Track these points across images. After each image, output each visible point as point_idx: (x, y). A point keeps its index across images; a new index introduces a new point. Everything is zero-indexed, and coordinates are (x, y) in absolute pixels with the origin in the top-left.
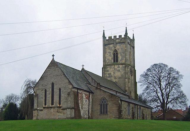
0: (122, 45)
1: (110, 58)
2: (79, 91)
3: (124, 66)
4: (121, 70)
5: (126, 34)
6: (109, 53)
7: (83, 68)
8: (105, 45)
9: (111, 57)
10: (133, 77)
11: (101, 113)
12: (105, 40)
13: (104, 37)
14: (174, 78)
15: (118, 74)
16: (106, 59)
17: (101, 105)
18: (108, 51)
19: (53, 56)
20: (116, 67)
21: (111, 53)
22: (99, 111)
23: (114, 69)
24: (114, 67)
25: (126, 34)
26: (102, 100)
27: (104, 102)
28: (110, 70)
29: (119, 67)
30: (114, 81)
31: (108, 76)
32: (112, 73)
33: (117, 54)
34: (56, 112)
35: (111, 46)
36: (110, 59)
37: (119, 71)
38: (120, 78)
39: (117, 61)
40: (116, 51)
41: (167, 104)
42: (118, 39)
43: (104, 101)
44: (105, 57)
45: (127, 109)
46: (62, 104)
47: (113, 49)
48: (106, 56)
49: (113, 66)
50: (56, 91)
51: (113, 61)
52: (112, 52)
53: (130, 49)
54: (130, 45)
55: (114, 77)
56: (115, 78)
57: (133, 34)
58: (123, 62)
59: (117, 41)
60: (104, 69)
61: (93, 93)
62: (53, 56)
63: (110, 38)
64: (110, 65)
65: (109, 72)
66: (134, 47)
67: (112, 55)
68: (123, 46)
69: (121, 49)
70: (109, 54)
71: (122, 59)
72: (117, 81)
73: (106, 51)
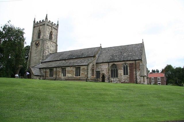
5: (46, 18)
7: (101, 46)
13: (34, 22)
25: (46, 18)
32: (49, 47)
40: (51, 32)
62: (101, 44)
63: (37, 22)
71: (54, 40)
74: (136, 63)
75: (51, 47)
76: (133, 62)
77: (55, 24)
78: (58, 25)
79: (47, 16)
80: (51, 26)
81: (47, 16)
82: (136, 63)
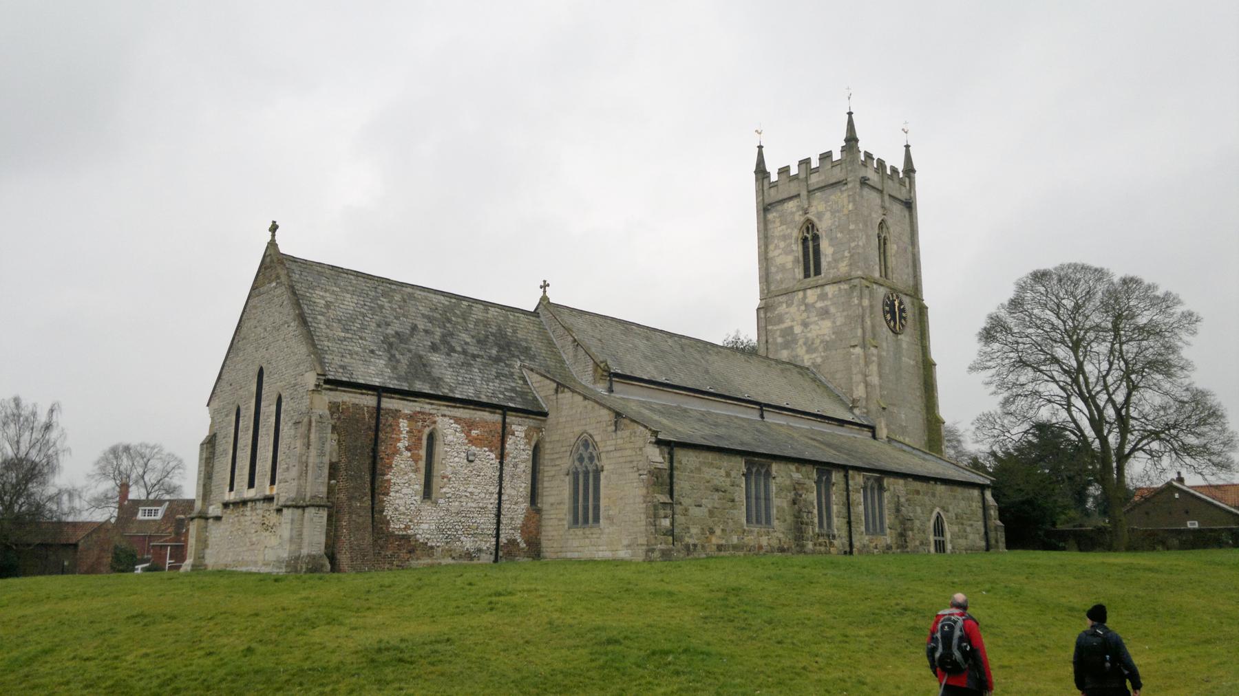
0: (833, 197)
1: (788, 257)
2: (389, 403)
3: (845, 286)
4: (833, 310)
5: (851, 140)
6: (784, 238)
8: (765, 208)
9: (790, 258)
10: (905, 339)
11: (576, 521)
12: (766, 187)
13: (761, 171)
14: (1150, 331)
15: (823, 329)
16: (773, 269)
17: (576, 475)
18: (777, 229)
19: (274, 228)
20: (812, 295)
21: (790, 236)
22: (565, 511)
23: (803, 308)
24: (805, 297)
25: (851, 140)
26: (578, 449)
27: (586, 460)
28: (791, 313)
29: (823, 297)
30: (807, 360)
31: (780, 340)
32: (798, 330)
33: (816, 238)
34: (259, 528)
35: (791, 206)
36: (789, 265)
37: (824, 313)
38: (828, 346)
39: (818, 272)
40: (810, 226)
41: (1123, 458)
42: (817, 170)
43: (586, 455)
44: (766, 259)
45: (740, 495)
46: (280, 483)
47: (799, 218)
48: (771, 255)
49: (801, 294)
50: (268, 409)
51: (799, 272)
52: (795, 233)
53: (881, 212)
54: (881, 192)
55: (805, 344)
56: (810, 349)
57: (850, 114)
58: (843, 268)
59: (815, 179)
60: (766, 311)
61: (545, 414)
63: (784, 171)
64: (788, 292)
65: (787, 324)
66: (909, 205)
67: (794, 247)
68: (841, 198)
69: (833, 213)
70: (782, 244)
72: (819, 360)
73: (770, 233)
74: (378, 408)
75: (805, 325)
76: (369, 400)
77: (894, 170)
78: (910, 170)
79: (760, 155)
80: (793, 189)
81: (760, 155)
82: (378, 408)
